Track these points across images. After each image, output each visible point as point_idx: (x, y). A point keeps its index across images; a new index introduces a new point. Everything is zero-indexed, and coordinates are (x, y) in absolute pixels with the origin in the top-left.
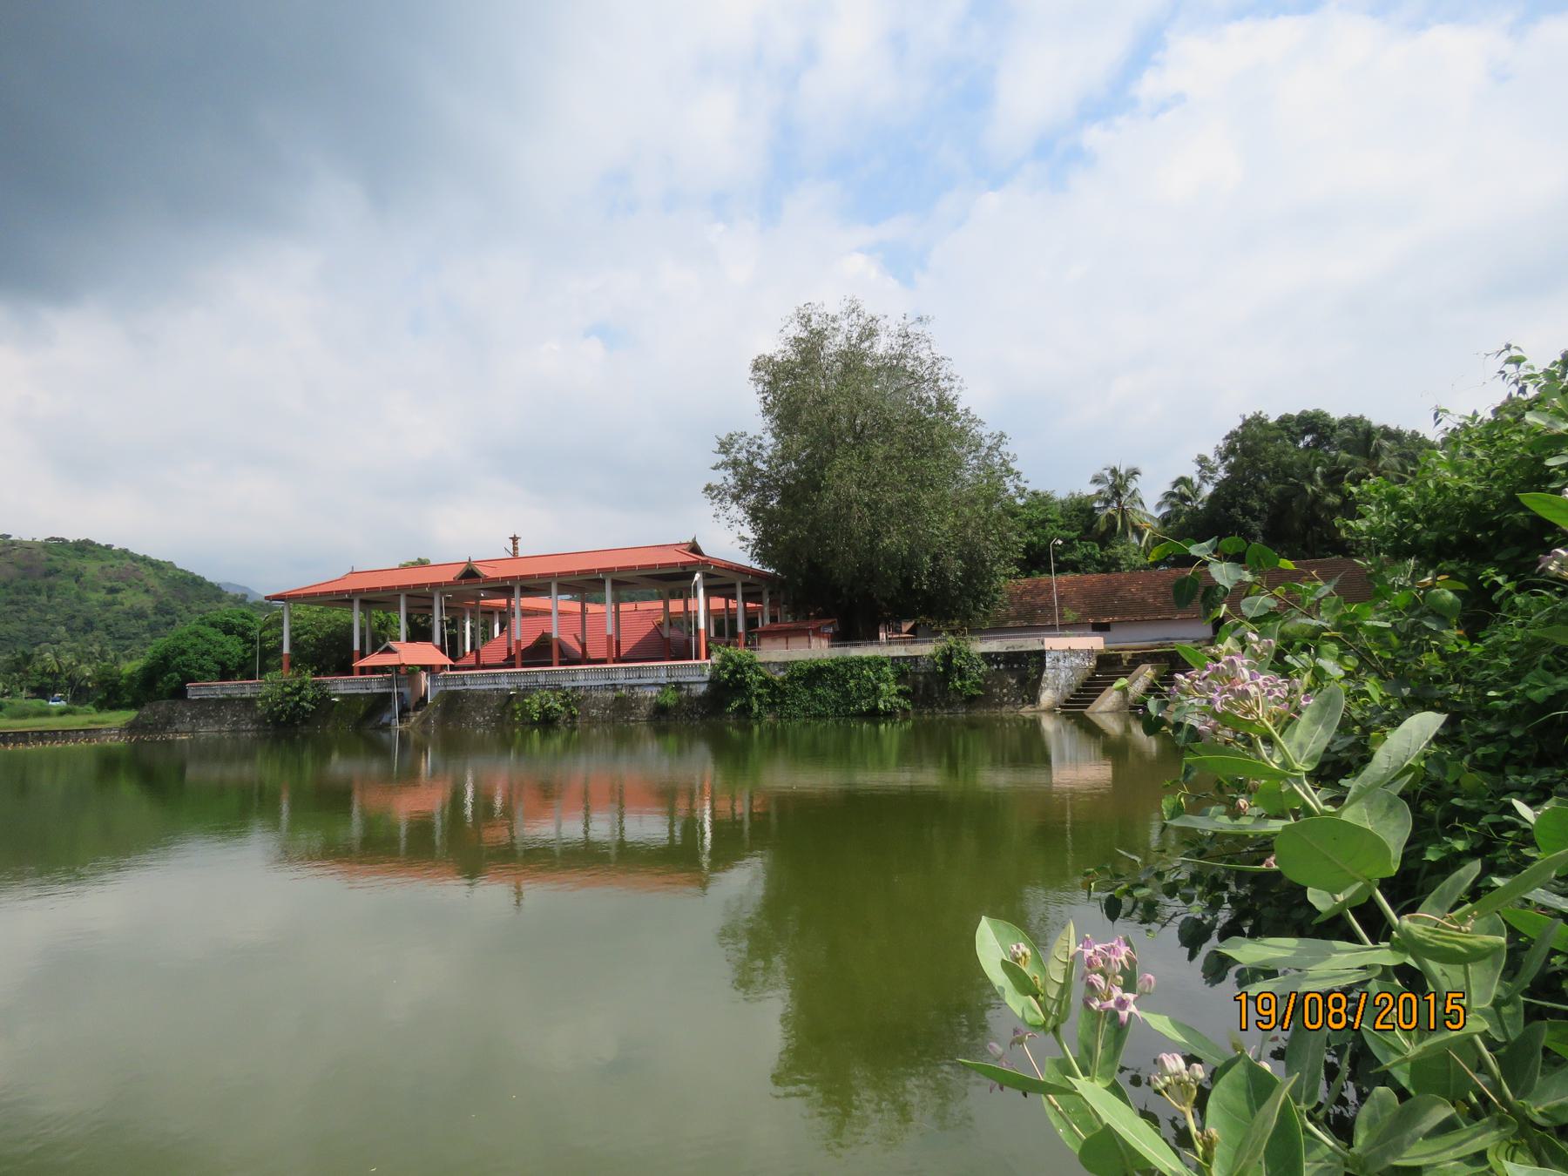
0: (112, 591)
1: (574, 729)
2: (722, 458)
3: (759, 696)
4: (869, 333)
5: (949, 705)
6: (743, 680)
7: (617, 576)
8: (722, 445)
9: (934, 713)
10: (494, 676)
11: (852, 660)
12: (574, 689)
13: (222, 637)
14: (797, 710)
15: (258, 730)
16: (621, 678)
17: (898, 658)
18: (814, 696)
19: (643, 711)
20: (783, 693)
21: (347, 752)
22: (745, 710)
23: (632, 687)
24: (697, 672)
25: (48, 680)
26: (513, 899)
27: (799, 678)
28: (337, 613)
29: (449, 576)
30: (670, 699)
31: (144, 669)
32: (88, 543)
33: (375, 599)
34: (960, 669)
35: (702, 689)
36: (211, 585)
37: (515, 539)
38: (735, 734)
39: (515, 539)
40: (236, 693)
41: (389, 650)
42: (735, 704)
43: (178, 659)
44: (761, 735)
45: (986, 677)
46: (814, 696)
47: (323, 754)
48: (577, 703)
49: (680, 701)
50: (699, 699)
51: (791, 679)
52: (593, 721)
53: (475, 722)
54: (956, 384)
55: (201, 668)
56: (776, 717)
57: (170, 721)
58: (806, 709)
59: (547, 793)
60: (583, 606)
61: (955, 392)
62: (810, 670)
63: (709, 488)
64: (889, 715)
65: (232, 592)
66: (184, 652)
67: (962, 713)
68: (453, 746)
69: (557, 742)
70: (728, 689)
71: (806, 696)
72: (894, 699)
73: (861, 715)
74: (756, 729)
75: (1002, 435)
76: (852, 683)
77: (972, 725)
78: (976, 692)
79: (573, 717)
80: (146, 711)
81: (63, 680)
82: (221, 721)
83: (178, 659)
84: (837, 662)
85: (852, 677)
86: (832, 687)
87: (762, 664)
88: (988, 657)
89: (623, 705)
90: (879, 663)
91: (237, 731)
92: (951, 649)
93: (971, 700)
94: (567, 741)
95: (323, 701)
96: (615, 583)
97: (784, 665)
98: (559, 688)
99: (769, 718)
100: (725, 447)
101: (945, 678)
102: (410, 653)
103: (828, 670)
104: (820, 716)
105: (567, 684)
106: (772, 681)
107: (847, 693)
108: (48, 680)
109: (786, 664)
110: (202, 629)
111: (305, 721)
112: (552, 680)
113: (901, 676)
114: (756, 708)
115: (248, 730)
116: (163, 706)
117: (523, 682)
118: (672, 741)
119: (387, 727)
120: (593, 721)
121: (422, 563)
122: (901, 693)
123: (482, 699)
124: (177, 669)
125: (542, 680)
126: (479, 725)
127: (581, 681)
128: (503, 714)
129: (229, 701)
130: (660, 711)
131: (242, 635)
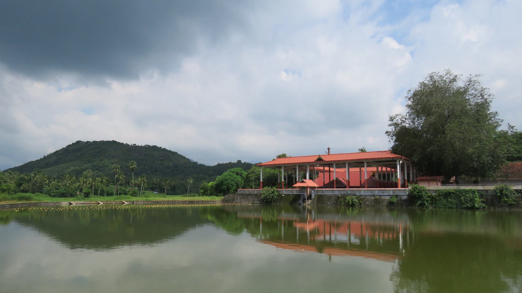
0: (162, 160)
1: (361, 208)
2: (391, 122)
3: (427, 200)
4: (454, 80)
5: (502, 206)
6: (421, 195)
7: (368, 161)
8: (391, 118)
9: (495, 209)
10: (333, 190)
11: (462, 190)
12: (360, 195)
13: (236, 176)
14: (441, 206)
15: (260, 203)
16: (376, 193)
17: (480, 190)
18: (448, 201)
19: (385, 203)
20: (436, 200)
21: (287, 211)
22: (422, 205)
23: (380, 196)
24: (403, 192)
25: (154, 186)
26: (328, 258)
27: (442, 195)
28: (276, 172)
29: (313, 160)
30: (395, 200)
31: (216, 184)
32: (155, 146)
33: (302, 166)
34: (506, 195)
35: (405, 197)
36: (187, 159)
37: (329, 149)
38: (419, 212)
39: (329, 149)
40: (252, 193)
41: (303, 182)
42: (419, 202)
43: (226, 182)
44: (428, 213)
45: (517, 198)
46: (448, 201)
47: (280, 212)
48: (362, 200)
49: (398, 201)
50: (404, 200)
51: (439, 195)
52: (367, 206)
53: (328, 204)
54: (491, 97)
55: (232, 185)
56: (434, 207)
57: (234, 200)
58: (445, 206)
59: (338, 226)
60: (360, 169)
61: (490, 100)
62: (446, 193)
63: (387, 132)
64: (477, 209)
65: (254, 163)
66: (227, 180)
67: (507, 209)
68: (320, 211)
69: (356, 212)
70: (414, 199)
71: (444, 201)
72: (480, 204)
73: (467, 208)
74: (427, 211)
75: (497, 113)
76: (462, 198)
77: (510, 213)
78: (513, 203)
79: (361, 204)
80: (226, 196)
81: (157, 186)
82: (249, 200)
83: (226, 182)
84: (456, 191)
85: (462, 196)
86: (455, 199)
87: (427, 190)
88: (517, 191)
89: (377, 201)
90: (473, 192)
91: (254, 203)
92: (503, 188)
93: (510, 205)
94: (359, 211)
95: (280, 195)
96: (349, 164)
97: (435, 191)
98: (355, 195)
99: (431, 208)
100: (392, 119)
101: (500, 198)
102: (309, 183)
103: (453, 193)
104: (450, 208)
105: (358, 194)
106: (432, 196)
107: (461, 201)
108: (154, 186)
109: (436, 190)
110: (231, 174)
111: (274, 201)
112: (352, 193)
113: (481, 196)
114: (426, 204)
115: (257, 203)
116: (231, 195)
117: (343, 193)
118: (395, 213)
119: (300, 204)
120: (367, 206)
121: (283, 156)
122: (482, 202)
123: (330, 197)
124: (225, 185)
125: (349, 192)
126: (329, 205)
127: (362, 193)
128: (337, 202)
129: (250, 195)
130: (391, 204)
131: (240, 175)
